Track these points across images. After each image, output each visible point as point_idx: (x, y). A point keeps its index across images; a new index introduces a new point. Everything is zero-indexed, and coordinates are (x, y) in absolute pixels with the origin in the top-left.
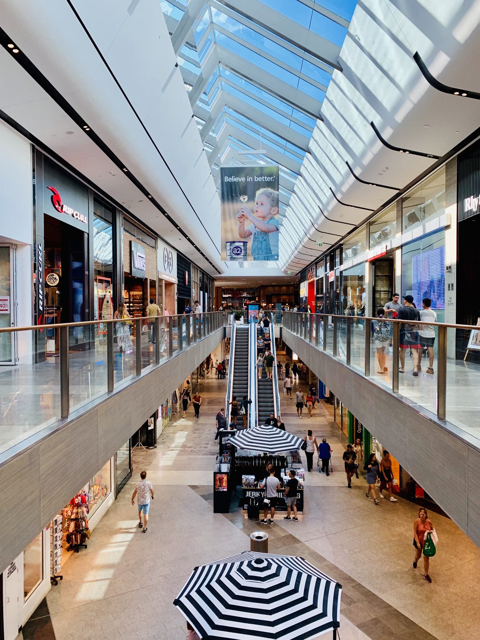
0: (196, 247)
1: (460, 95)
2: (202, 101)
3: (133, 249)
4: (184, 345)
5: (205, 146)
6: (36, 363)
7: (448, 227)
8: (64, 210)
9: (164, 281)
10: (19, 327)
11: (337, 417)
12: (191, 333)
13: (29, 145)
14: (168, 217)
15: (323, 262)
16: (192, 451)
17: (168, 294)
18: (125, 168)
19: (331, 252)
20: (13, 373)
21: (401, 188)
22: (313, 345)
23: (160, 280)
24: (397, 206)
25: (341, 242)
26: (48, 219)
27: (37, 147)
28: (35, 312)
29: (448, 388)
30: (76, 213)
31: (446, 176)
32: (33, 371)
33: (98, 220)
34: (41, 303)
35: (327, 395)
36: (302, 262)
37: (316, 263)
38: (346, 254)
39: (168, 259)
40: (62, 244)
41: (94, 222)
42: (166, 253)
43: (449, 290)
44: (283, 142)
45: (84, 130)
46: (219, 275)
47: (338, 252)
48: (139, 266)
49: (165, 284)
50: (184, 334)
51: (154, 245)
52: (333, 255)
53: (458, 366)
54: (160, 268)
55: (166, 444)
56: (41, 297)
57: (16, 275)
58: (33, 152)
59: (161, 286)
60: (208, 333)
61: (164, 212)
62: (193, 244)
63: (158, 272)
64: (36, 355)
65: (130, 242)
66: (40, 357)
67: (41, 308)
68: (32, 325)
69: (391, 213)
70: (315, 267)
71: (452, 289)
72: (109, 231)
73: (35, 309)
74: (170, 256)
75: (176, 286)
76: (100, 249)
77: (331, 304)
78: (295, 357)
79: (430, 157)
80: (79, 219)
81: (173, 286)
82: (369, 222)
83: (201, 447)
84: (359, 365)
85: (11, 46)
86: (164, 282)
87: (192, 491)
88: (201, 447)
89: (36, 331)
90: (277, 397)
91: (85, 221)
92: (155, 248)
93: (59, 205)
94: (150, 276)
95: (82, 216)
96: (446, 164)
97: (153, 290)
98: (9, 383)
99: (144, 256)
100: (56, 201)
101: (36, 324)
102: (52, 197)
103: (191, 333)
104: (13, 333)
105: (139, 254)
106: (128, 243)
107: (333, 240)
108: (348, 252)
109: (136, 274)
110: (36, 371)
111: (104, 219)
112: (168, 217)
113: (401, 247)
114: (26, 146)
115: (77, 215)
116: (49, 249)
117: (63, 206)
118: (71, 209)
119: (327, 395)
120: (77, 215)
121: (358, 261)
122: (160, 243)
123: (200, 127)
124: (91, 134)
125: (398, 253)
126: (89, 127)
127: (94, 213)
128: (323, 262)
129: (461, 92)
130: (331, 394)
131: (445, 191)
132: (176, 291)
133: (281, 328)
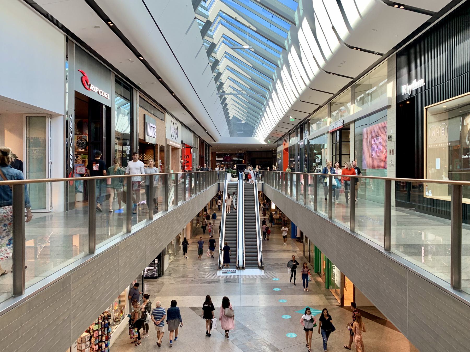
0: (197, 121)
1: (399, 7)
2: (203, 7)
3: (146, 121)
4: (187, 195)
5: (204, 42)
6: (67, 210)
7: (389, 107)
8: (91, 88)
9: (171, 147)
10: (53, 178)
11: (305, 253)
12: (193, 185)
13: (63, 36)
14: (175, 97)
15: (295, 132)
16: (192, 280)
17: (174, 157)
18: (141, 56)
19: (301, 126)
20: (47, 218)
21: (355, 77)
22: (289, 196)
23: (168, 146)
24: (352, 90)
25: (309, 118)
26: (77, 94)
27: (69, 37)
28: (67, 171)
29: (392, 227)
30: (101, 91)
31: (388, 68)
32: (64, 217)
33: (119, 98)
34: (71, 162)
35: (298, 235)
36: (278, 133)
37: (290, 134)
38: (312, 128)
39: (174, 129)
40: (89, 114)
41: (116, 99)
42: (172, 124)
43: (390, 154)
44: (265, 40)
45: (109, 25)
46: (214, 143)
47: (306, 126)
48: (151, 134)
49: (172, 149)
50: (187, 186)
51: (163, 119)
52: (302, 127)
53: (398, 212)
54: (168, 136)
55: (172, 275)
56: (71, 157)
57: (51, 140)
58: (67, 41)
59: (168, 151)
60: (206, 188)
61: (171, 92)
62: (194, 118)
63: (166, 140)
64: (67, 204)
65: (145, 115)
66: (69, 205)
67: (71, 166)
68: (64, 177)
69: (347, 94)
70: (288, 137)
71: (393, 154)
72: (127, 107)
73: (67, 168)
74: (176, 127)
75: (180, 150)
76: (120, 124)
77: (305, 158)
78: (273, 206)
79: (376, 54)
80: (103, 96)
81: (178, 150)
82: (329, 103)
83: (200, 277)
84: (322, 211)
85: (111, 25)
86: (171, 147)
87: (193, 312)
88: (200, 277)
89: (67, 182)
90: (259, 238)
91: (108, 98)
92: (163, 120)
93: (88, 85)
94: (161, 143)
95: (106, 93)
96: (388, 60)
97: (162, 154)
98: (44, 226)
99: (155, 127)
100: (85, 83)
101: (67, 177)
102: (82, 78)
103: (193, 185)
104: (47, 184)
105: (151, 125)
106: (143, 116)
107: (303, 116)
108: (314, 127)
109: (150, 140)
110: (67, 217)
111: (124, 97)
112: (175, 97)
113: (355, 121)
114: (61, 37)
115: (101, 93)
116: (79, 120)
117: (90, 85)
118: (97, 88)
119: (298, 235)
120: (101, 93)
121: (322, 130)
122: (168, 117)
123: (201, 27)
124: (115, 29)
125: (352, 126)
126: (112, 23)
127: (116, 92)
128: (295, 132)
129: (400, 5)
130: (301, 234)
131: (387, 80)
132: (180, 155)
133: (262, 184)
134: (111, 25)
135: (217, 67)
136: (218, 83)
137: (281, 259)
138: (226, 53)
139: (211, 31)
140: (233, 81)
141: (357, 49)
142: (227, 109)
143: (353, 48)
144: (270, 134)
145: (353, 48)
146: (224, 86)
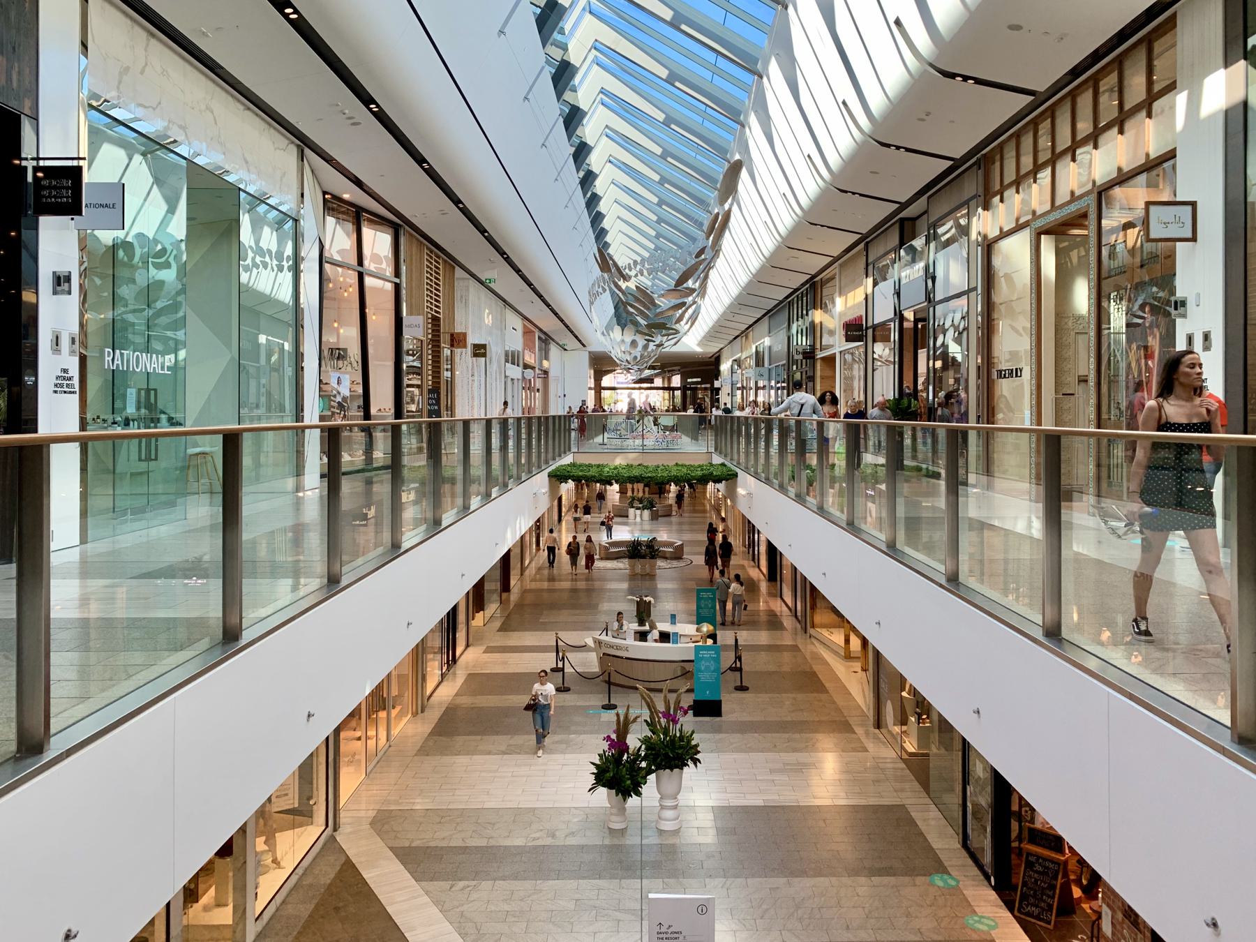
85: (294, 16)
134: (294, 16)
135: (578, 132)
136: (582, 174)
137: (692, 531)
138: (603, 91)
139: (562, 32)
140: (625, 142)
141: (966, 78)
142: (607, 245)
143: (952, 76)
144: (713, 327)
145: (952, 76)
146: (598, 182)
